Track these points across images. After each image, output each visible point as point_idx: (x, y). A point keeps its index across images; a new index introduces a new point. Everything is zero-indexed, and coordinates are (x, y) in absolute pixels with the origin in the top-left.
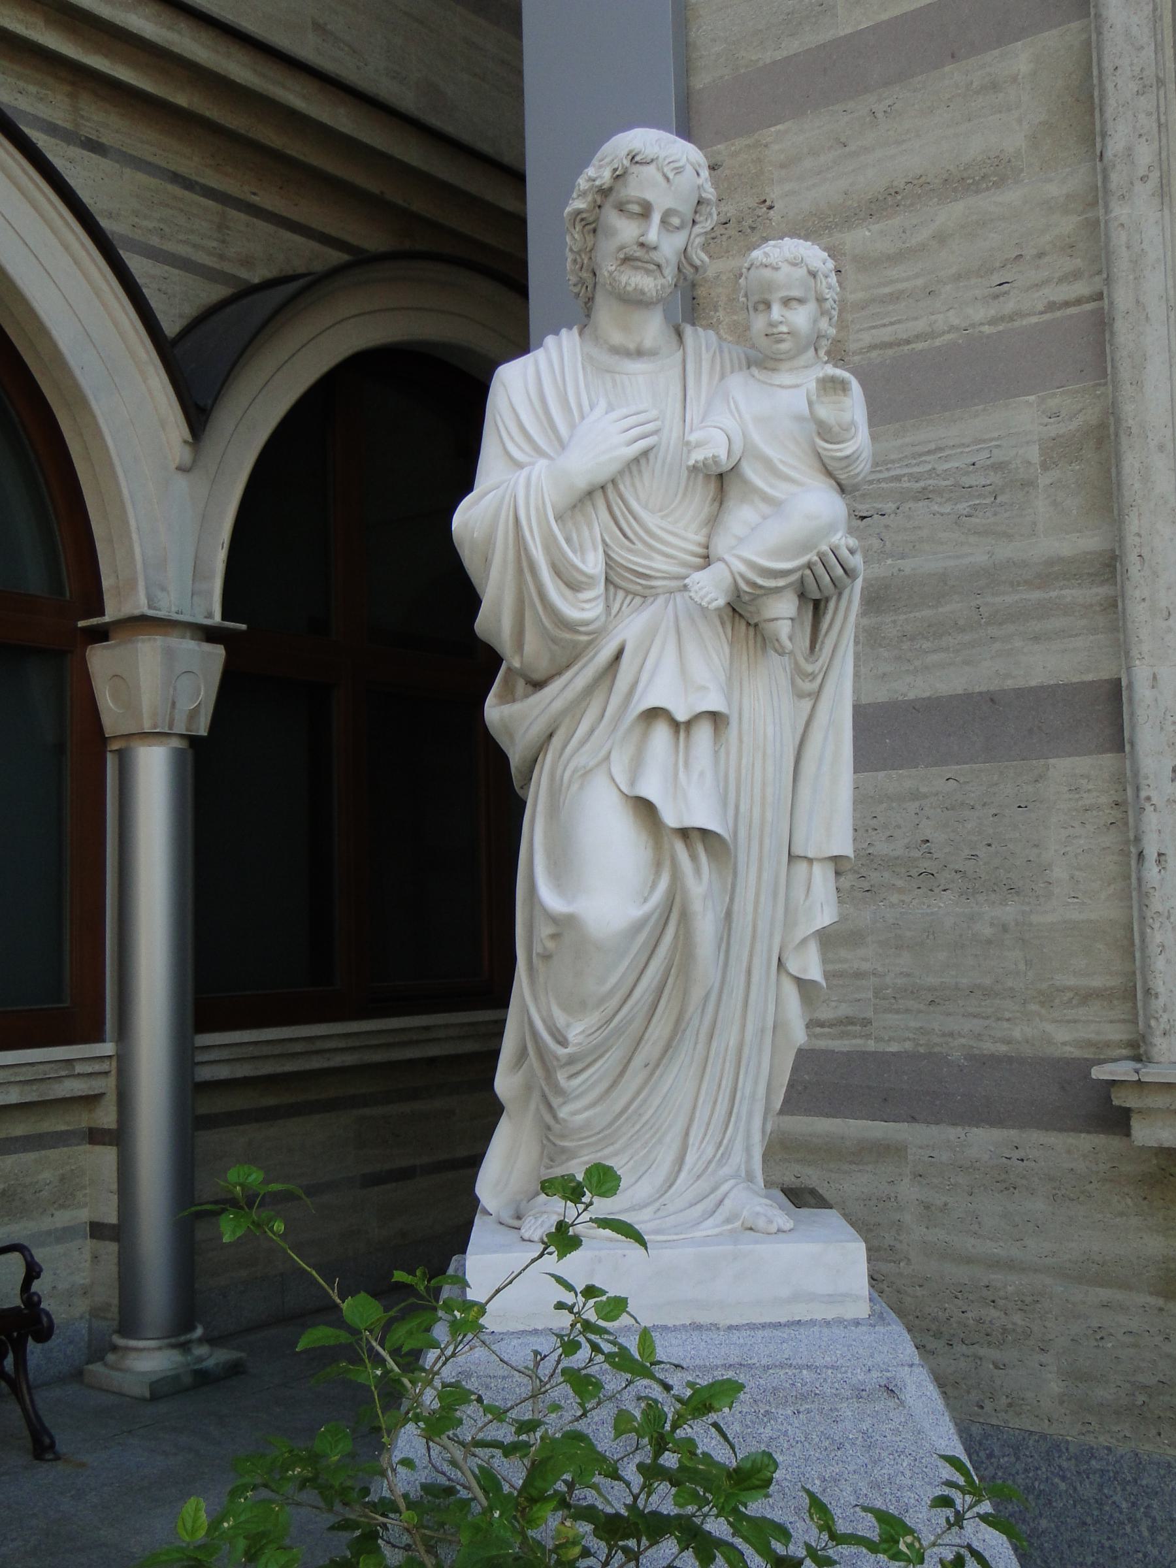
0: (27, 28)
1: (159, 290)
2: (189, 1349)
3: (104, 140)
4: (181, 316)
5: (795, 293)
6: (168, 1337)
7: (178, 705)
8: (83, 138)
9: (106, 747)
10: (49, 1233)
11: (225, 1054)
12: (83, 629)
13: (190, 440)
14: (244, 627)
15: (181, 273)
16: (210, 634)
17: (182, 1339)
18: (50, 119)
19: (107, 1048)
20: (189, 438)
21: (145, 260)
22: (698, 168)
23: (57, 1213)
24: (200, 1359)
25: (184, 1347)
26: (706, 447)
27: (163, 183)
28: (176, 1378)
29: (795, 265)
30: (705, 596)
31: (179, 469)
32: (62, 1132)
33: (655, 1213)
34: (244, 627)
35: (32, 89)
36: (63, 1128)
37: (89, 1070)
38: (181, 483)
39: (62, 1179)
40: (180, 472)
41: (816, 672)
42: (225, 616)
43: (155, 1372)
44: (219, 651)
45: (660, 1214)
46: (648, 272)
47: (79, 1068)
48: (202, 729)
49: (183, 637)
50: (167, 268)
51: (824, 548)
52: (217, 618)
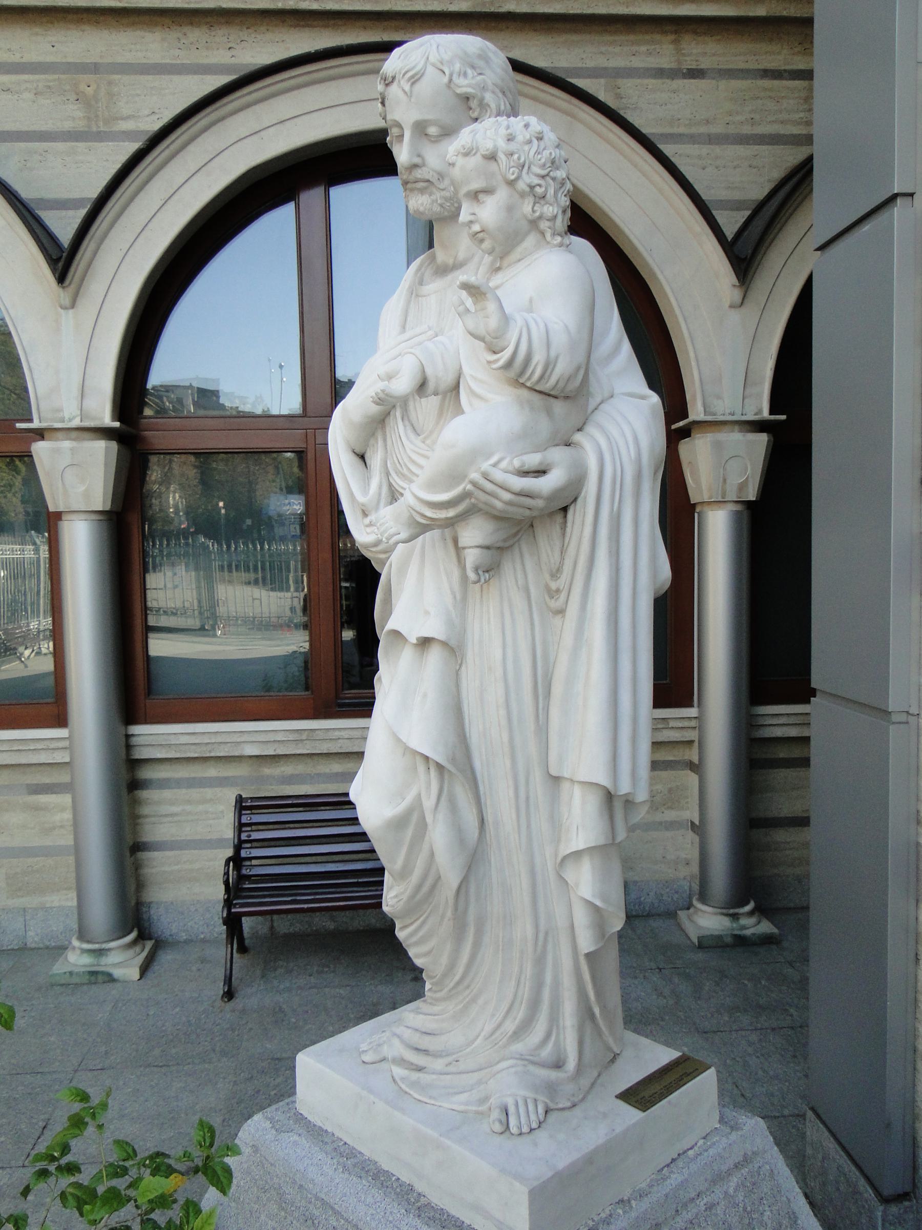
0: (627, 7)
1: (750, 166)
2: (738, 919)
3: (702, 66)
4: (769, 181)
5: (475, 185)
6: (722, 908)
7: (728, 481)
8: (685, 71)
9: (695, 510)
10: (661, 823)
11: (792, 720)
12: (675, 430)
13: (738, 284)
14: (784, 417)
15: (770, 147)
16: (759, 426)
17: (732, 911)
18: (657, 66)
19: (692, 712)
20: (736, 282)
21: (737, 147)
22: (441, 67)
23: (666, 811)
24: (744, 928)
25: (735, 917)
26: (399, 376)
27: (753, 81)
28: (720, 937)
29: (466, 155)
30: (385, 531)
31: (731, 307)
32: (671, 761)
33: (447, 1066)
34: (784, 417)
35: (643, 48)
36: (671, 758)
37: (680, 725)
38: (735, 317)
39: (670, 790)
40: (733, 310)
41: (561, 588)
42: (772, 412)
43: (709, 929)
44: (763, 438)
45: (451, 1069)
46: (422, 191)
47: (672, 724)
48: (752, 494)
49: (733, 431)
50: (757, 147)
51: (475, 476)
52: (766, 414)
